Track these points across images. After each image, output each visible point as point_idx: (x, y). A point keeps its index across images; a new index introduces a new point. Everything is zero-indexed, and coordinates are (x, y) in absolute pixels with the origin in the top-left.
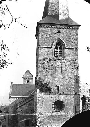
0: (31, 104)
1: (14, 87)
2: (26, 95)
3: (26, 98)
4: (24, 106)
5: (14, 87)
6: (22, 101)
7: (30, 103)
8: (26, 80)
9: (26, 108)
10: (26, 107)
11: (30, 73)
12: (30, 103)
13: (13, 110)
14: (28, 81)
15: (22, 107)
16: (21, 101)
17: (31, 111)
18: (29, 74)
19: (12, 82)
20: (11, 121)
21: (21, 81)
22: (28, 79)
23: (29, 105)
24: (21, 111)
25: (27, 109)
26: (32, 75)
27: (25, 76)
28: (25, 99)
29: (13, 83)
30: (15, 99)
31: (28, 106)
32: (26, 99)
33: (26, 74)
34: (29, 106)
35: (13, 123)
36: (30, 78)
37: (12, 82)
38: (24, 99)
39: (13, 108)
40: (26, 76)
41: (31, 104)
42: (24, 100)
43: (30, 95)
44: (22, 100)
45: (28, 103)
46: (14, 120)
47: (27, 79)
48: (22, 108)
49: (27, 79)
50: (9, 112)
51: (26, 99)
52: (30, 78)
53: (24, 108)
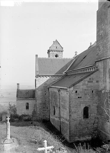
0: (93, 79)
1: (40, 61)
2: (60, 72)
3: (60, 76)
4: (81, 83)
5: (40, 61)
6: (55, 81)
7: (90, 79)
8: (54, 53)
9: (85, 87)
10: (83, 85)
11: (59, 44)
12: (90, 79)
13: (42, 95)
14: (56, 56)
15: (77, 85)
16: (54, 80)
17: (93, 91)
18: (58, 46)
19: (37, 56)
20: (39, 110)
21: (44, 55)
22: (56, 52)
23: (88, 82)
24: (76, 92)
25: (85, 90)
26: (62, 47)
27: (52, 49)
28: (59, 78)
29: (39, 57)
30: (48, 78)
31: (86, 83)
32: (60, 77)
33: (54, 45)
34: (89, 84)
35: (43, 113)
36: (59, 51)
37: (37, 56)
38: (57, 78)
39: (42, 90)
40: (54, 49)
41: (91, 80)
42: (58, 79)
43: (65, 72)
44: (55, 79)
45: (88, 79)
46: (44, 108)
47: (56, 53)
48: (78, 87)
49: (56, 53)
50: (36, 96)
51: (60, 77)
52: (59, 51)
53: (82, 87)
